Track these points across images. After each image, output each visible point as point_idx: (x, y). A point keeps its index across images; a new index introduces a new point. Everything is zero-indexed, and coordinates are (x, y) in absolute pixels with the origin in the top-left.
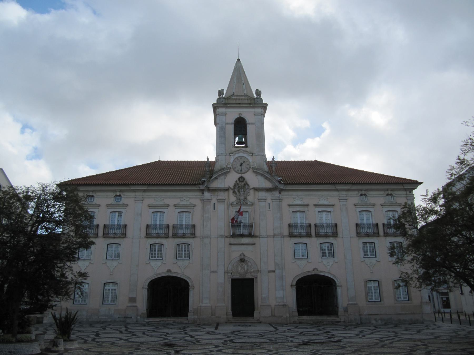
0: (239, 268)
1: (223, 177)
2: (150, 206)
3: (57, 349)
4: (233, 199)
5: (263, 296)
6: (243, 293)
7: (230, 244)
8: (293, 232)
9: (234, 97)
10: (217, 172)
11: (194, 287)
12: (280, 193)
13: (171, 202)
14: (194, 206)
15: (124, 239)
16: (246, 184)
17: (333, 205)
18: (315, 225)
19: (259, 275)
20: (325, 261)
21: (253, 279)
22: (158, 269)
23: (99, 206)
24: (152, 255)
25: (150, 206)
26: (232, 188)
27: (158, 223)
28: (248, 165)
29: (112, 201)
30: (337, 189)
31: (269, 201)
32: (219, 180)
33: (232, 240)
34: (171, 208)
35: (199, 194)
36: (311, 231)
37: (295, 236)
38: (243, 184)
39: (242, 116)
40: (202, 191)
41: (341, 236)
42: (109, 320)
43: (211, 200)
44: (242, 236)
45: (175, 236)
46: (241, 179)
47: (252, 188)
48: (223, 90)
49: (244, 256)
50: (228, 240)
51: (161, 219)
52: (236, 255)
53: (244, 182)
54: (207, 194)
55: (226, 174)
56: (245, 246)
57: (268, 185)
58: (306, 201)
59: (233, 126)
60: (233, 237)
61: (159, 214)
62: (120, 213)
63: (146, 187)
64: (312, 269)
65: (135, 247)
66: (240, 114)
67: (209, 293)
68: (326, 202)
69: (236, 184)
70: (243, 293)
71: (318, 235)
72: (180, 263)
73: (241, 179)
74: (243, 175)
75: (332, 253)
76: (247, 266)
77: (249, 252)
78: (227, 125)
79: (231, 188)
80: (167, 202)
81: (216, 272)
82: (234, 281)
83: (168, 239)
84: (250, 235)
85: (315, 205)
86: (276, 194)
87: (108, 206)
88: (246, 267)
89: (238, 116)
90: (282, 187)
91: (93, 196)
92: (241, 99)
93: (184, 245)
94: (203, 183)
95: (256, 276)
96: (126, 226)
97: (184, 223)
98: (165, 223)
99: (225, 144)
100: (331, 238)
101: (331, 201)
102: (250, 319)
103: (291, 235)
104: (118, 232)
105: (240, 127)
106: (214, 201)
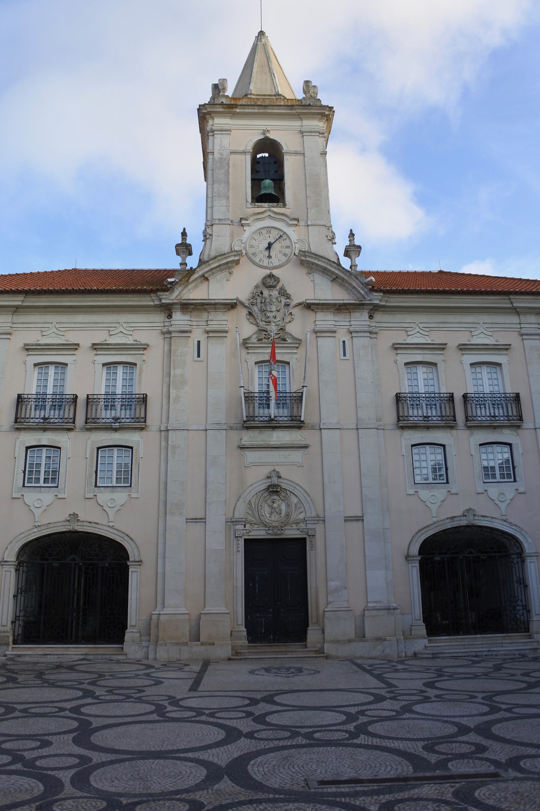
0: (266, 510)
2: (28, 348)
6: (277, 580)
7: (242, 448)
8: (406, 413)
12: (371, 317)
13: (85, 339)
14: (145, 347)
17: (506, 348)
20: (494, 491)
21: (305, 539)
22: (440, 509)
24: (30, 475)
27: (50, 391)
28: (287, 247)
30: (515, 308)
31: (342, 335)
33: (249, 437)
34: (452, 353)
35: (158, 319)
36: (449, 412)
37: (414, 427)
40: (168, 310)
41: (531, 426)
43: (190, 332)
44: (272, 425)
45: (92, 425)
46: (270, 281)
47: (300, 304)
49: (279, 477)
50: (234, 435)
51: (129, 381)
52: (257, 478)
54: (180, 319)
56: (283, 453)
58: (437, 338)
60: (248, 428)
61: (120, 369)
64: (460, 513)
67: (186, 581)
69: (257, 294)
70: (277, 580)
71: (472, 424)
73: (270, 281)
74: (275, 272)
75: (509, 471)
76: (288, 506)
77: (292, 468)
78: (232, 157)
79: (242, 304)
80: (72, 338)
83: (72, 434)
84: (296, 423)
85: (463, 348)
86: (360, 319)
88: (283, 507)
89: (262, 137)
97: (119, 390)
98: (69, 390)
99: (228, 198)
100: (507, 432)
101: (502, 339)
103: (403, 424)
106: (198, 335)
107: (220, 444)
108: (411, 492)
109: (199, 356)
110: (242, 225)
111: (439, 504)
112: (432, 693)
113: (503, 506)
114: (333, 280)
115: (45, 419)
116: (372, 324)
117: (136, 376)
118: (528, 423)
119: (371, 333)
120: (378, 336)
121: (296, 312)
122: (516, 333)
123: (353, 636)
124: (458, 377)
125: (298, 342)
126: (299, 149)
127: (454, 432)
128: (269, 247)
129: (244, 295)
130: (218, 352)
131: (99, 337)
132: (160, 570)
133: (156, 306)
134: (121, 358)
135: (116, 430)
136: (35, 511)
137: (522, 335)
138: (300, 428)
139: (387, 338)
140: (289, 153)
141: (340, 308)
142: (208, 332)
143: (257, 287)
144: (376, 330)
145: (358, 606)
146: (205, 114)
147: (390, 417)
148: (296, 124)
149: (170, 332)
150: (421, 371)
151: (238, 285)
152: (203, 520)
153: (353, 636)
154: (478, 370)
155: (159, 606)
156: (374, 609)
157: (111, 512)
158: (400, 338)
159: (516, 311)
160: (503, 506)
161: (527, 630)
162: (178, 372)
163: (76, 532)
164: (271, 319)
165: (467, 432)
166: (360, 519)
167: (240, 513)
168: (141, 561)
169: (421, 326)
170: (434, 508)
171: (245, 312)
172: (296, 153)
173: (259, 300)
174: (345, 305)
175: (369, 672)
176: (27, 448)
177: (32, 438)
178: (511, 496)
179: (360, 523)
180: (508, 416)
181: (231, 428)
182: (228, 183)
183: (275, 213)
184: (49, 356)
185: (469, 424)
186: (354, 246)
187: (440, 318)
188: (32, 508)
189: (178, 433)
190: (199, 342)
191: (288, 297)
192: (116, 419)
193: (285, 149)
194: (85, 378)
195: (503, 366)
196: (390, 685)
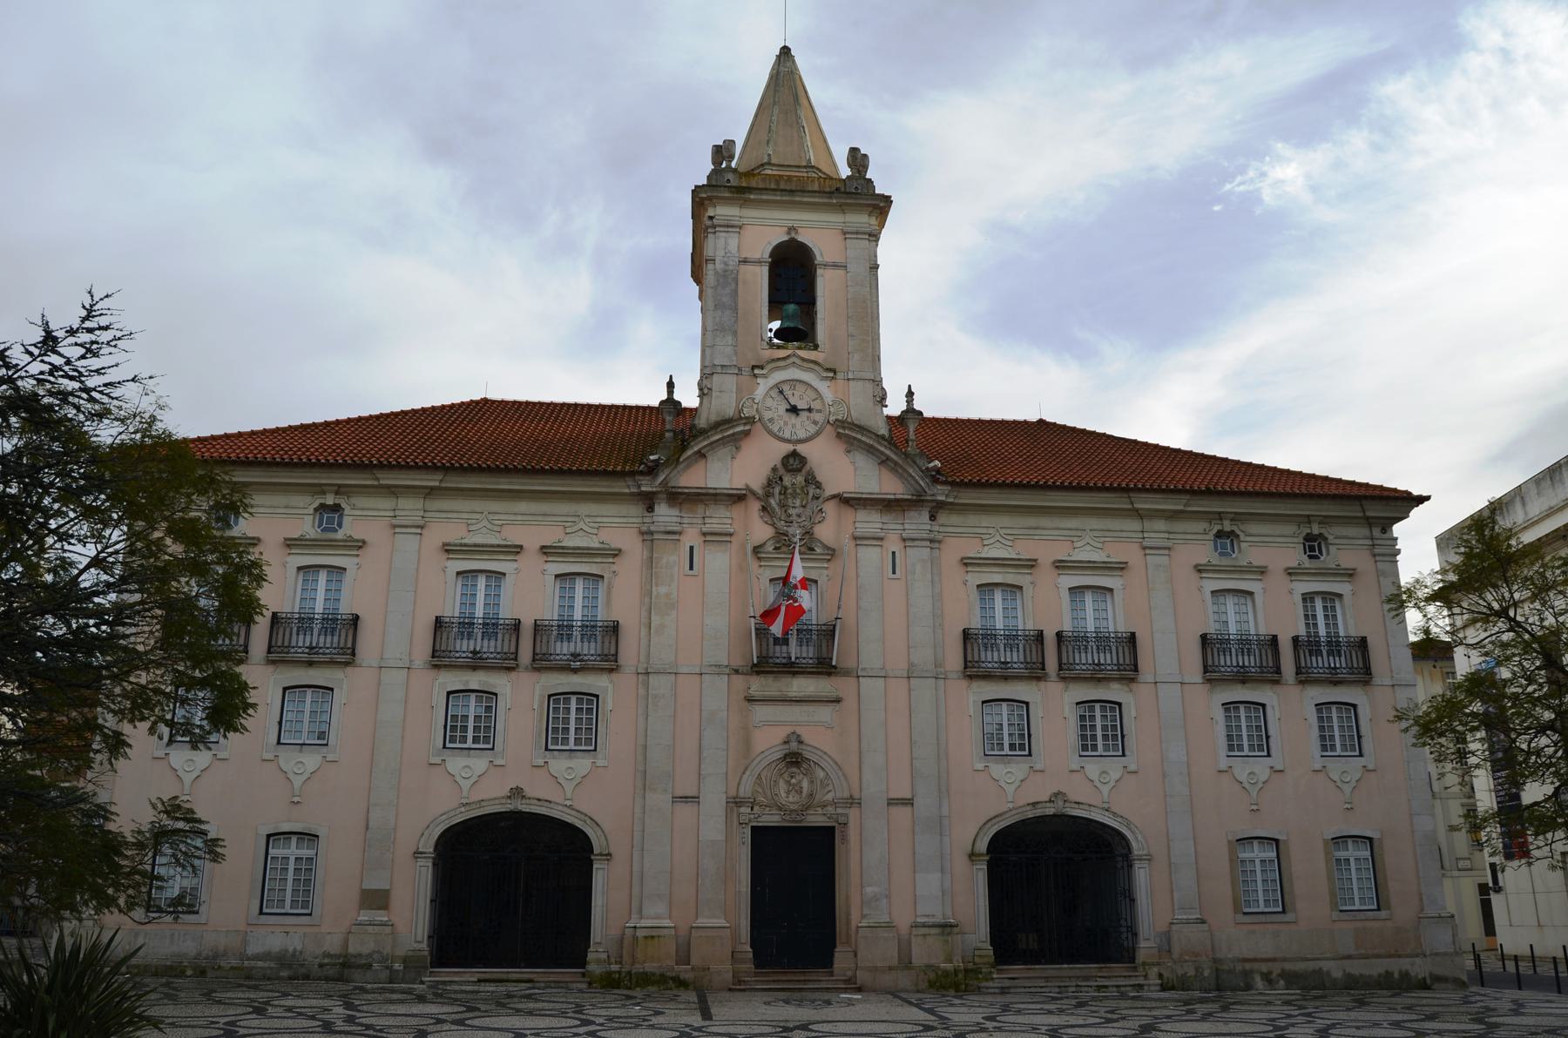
2: (449, 549)
5: (869, 890)
6: (794, 887)
7: (750, 700)
8: (978, 656)
12: (933, 518)
14: (616, 553)
17: (1121, 568)
24: (454, 731)
31: (893, 544)
33: (758, 685)
34: (1045, 574)
35: (634, 511)
36: (1039, 657)
37: (987, 677)
40: (648, 502)
44: (791, 669)
45: (542, 663)
46: (794, 462)
47: (834, 497)
49: (801, 742)
54: (665, 514)
58: (1024, 550)
60: (758, 673)
69: (774, 480)
70: (794, 887)
71: (1067, 674)
73: (794, 462)
74: (800, 448)
77: (819, 731)
78: (743, 268)
79: (753, 493)
80: (513, 535)
84: (824, 667)
85: (1060, 566)
86: (918, 522)
88: (805, 784)
89: (786, 238)
98: (506, 613)
99: (735, 333)
100: (1115, 686)
101: (1115, 553)
103: (973, 671)
106: (691, 537)
107: (719, 694)
108: (980, 766)
109: (691, 568)
110: (755, 376)
111: (1017, 783)
112: (990, 1025)
113: (1105, 790)
114: (882, 463)
115: (474, 652)
116: (936, 528)
117: (601, 594)
118: (1146, 674)
119: (931, 541)
120: (943, 546)
121: (830, 508)
122: (1136, 546)
123: (895, 962)
124: (1048, 607)
125: (831, 553)
126: (839, 259)
127: (1042, 684)
128: (794, 410)
129: (757, 484)
130: (718, 564)
131: (551, 536)
132: (636, 868)
133: (632, 494)
134: (582, 566)
135: (575, 671)
136: (462, 782)
137: (1144, 548)
138: (829, 674)
139: (956, 548)
140: (826, 265)
141: (888, 505)
142: (704, 534)
143: (774, 469)
144: (940, 537)
145: (903, 921)
146: (703, 199)
147: (954, 660)
148: (836, 218)
149: (652, 533)
150: (1230, 603)
151: (746, 467)
152: (693, 799)
153: (895, 962)
154: (1221, 599)
155: (634, 916)
156: (924, 925)
157: (569, 787)
158: (973, 549)
159: (1139, 515)
160: (1105, 790)
161: (1132, 960)
162: (663, 590)
163: (520, 813)
164: (794, 518)
165: (1061, 685)
166: (908, 802)
167: (746, 790)
168: (609, 854)
169: (1002, 532)
170: (1010, 789)
171: (755, 506)
172: (835, 266)
173: (777, 490)
174: (897, 500)
175: (917, 1006)
176: (449, 693)
177: (455, 680)
178: (1117, 776)
179: (909, 808)
180: (1118, 664)
181: (737, 672)
182: (735, 310)
183: (803, 360)
184: (479, 562)
185: (1066, 673)
186: (914, 411)
187: (1031, 521)
188: (458, 778)
189: (663, 678)
190: (692, 548)
191: (818, 485)
192: (575, 656)
193: (819, 259)
194: (529, 595)
195: (1256, 596)
196: (942, 1018)
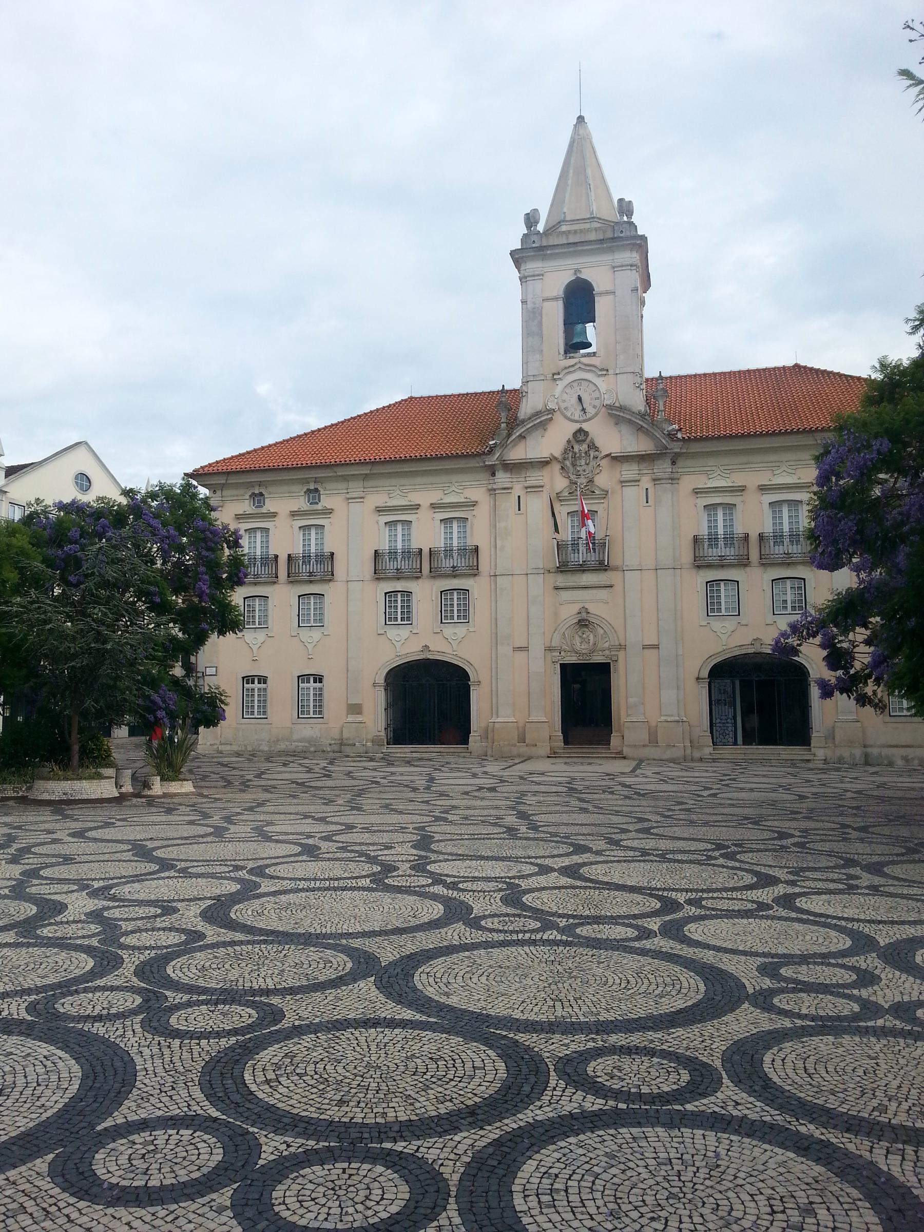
0: (577, 641)
1: (540, 432)
3: (149, 793)
4: (561, 483)
5: (631, 700)
6: (587, 699)
7: (557, 588)
9: (564, 228)
10: (523, 421)
11: (479, 683)
12: (674, 463)
14: (474, 504)
15: (331, 584)
16: (593, 446)
18: (761, 537)
19: (621, 654)
23: (274, 515)
25: (380, 510)
26: (560, 458)
28: (597, 399)
29: (301, 503)
32: (530, 441)
33: (561, 580)
35: (484, 476)
37: (709, 566)
38: (584, 447)
39: (583, 276)
42: (312, 749)
46: (580, 435)
47: (607, 456)
48: (535, 211)
52: (569, 613)
53: (588, 440)
54: (502, 478)
55: (543, 425)
57: (644, 445)
58: (738, 479)
59: (560, 305)
62: (730, 507)
63: (369, 467)
65: (355, 598)
66: (577, 271)
68: (404, 502)
69: (569, 447)
70: (587, 699)
71: (766, 562)
72: (448, 631)
74: (586, 426)
77: (599, 606)
78: (546, 304)
80: (415, 497)
81: (525, 649)
82: (563, 667)
84: (602, 567)
85: (763, 489)
87: (294, 514)
90: (676, 448)
91: (261, 494)
92: (581, 231)
93: (455, 593)
94: (491, 451)
95: (614, 658)
96: (476, 549)
100: (801, 567)
102: (601, 749)
104: (313, 570)
105: (579, 302)
106: (518, 490)
